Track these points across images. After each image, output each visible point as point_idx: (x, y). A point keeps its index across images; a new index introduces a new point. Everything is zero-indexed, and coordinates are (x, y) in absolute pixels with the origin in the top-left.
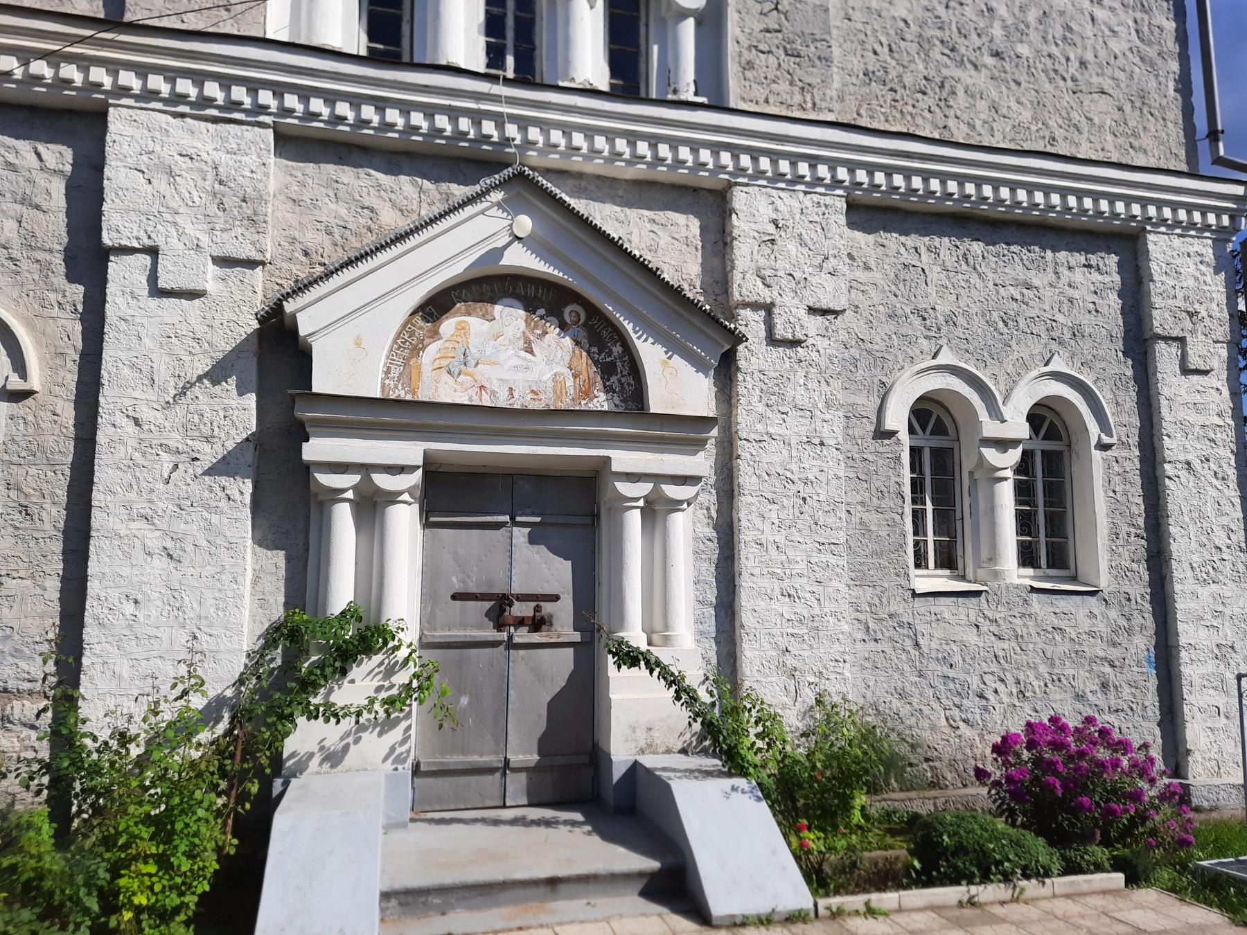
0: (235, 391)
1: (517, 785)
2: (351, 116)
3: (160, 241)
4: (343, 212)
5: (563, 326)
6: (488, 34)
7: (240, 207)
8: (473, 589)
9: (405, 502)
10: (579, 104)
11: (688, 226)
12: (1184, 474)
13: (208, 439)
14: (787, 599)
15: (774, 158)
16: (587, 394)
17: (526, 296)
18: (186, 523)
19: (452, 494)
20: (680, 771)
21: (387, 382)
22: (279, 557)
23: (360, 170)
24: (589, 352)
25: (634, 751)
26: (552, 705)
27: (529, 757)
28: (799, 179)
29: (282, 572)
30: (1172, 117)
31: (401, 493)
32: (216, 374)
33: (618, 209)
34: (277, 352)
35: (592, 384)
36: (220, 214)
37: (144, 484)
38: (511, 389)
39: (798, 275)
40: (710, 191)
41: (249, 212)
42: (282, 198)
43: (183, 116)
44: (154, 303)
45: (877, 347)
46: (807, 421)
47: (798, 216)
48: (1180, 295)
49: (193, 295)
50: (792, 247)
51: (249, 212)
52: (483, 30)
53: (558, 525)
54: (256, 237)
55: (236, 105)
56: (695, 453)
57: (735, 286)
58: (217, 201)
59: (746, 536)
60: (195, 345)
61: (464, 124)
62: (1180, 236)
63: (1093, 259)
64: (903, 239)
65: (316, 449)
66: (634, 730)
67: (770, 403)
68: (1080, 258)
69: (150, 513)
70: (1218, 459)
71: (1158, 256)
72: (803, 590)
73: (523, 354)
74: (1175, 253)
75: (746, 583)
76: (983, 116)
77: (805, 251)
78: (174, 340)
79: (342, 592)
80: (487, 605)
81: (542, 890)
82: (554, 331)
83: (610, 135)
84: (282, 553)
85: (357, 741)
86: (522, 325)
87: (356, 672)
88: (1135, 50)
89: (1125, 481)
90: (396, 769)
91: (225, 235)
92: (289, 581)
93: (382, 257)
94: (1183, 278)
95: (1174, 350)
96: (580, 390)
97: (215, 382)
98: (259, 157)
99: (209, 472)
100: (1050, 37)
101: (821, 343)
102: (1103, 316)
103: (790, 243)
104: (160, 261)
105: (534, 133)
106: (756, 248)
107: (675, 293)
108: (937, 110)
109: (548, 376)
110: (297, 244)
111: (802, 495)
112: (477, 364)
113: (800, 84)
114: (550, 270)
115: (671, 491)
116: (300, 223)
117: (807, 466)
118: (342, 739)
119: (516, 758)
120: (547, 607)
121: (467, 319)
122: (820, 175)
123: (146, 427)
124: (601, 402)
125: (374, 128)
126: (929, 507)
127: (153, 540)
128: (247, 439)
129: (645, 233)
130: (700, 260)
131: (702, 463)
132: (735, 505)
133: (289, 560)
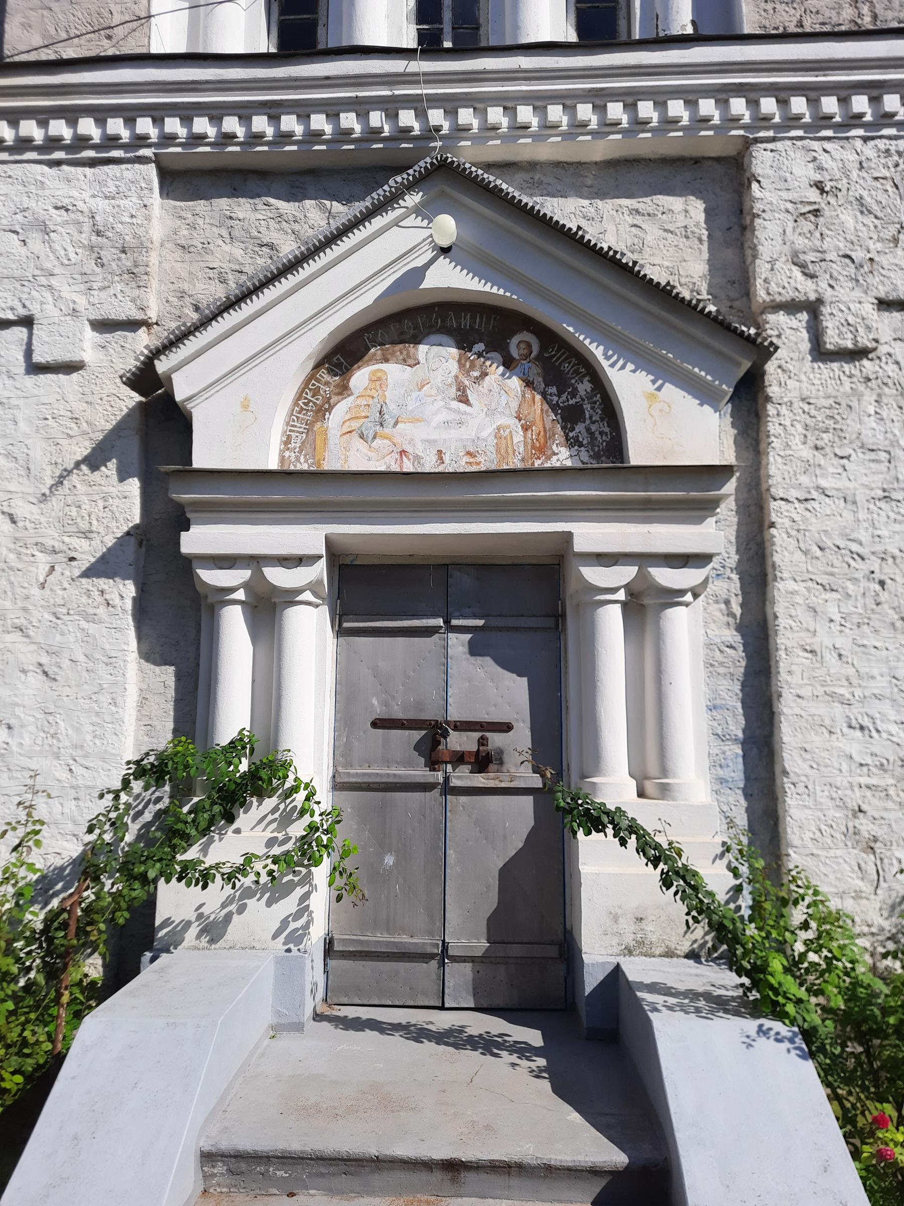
0: (115, 477)
1: (459, 978)
2: (240, 132)
3: (35, 309)
4: (238, 252)
5: (508, 363)
6: (419, 21)
7: (119, 259)
8: (399, 714)
10: (524, 66)
11: (688, 211)
13: (86, 534)
14: (858, 733)
15: (812, 95)
16: (542, 450)
17: (459, 328)
18: (62, 634)
19: (366, 591)
20: (676, 994)
21: (287, 454)
22: (168, 674)
23: (257, 201)
24: (544, 395)
25: (616, 950)
26: (505, 872)
27: (474, 943)
28: (855, 120)
29: (171, 693)
31: (299, 591)
32: (94, 461)
33: (586, 202)
34: (158, 427)
35: (548, 436)
36: (98, 270)
37: (19, 590)
38: (440, 452)
40: (718, 160)
41: (129, 264)
42: (169, 245)
43: (58, 163)
44: (31, 381)
46: (883, 467)
47: (854, 174)
49: (71, 367)
50: (848, 218)
51: (129, 264)
52: (413, 17)
53: (508, 629)
54: (136, 292)
55: (112, 141)
56: (700, 521)
57: (759, 282)
58: (95, 255)
59: (788, 639)
60: (73, 425)
61: (376, 118)
65: (197, 539)
66: (616, 919)
67: (820, 443)
69: (25, 622)
72: (885, 719)
73: (455, 404)
75: (789, 709)
77: (869, 220)
78: (51, 422)
79: (233, 716)
80: (417, 735)
81: (437, 1176)
82: (496, 371)
83: (568, 101)
84: (171, 669)
85: (241, 910)
86: (454, 367)
87: (244, 820)
90: (289, 950)
91: (103, 295)
92: (180, 702)
93: (270, 294)
96: (533, 447)
97: (94, 467)
99: (89, 573)
104: (35, 331)
105: (466, 116)
106: (791, 224)
107: (663, 294)
109: (488, 431)
110: (187, 299)
111: (877, 576)
112: (396, 423)
114: (487, 288)
115: (665, 576)
116: (190, 273)
117: (884, 532)
118: (224, 906)
119: (458, 943)
120: (496, 740)
121: (384, 366)
122: (888, 108)
123: (20, 524)
124: (562, 457)
125: (268, 143)
127: (28, 655)
128: (128, 533)
129: (625, 229)
130: (706, 255)
131: (716, 534)
132: (769, 596)
133: (179, 677)
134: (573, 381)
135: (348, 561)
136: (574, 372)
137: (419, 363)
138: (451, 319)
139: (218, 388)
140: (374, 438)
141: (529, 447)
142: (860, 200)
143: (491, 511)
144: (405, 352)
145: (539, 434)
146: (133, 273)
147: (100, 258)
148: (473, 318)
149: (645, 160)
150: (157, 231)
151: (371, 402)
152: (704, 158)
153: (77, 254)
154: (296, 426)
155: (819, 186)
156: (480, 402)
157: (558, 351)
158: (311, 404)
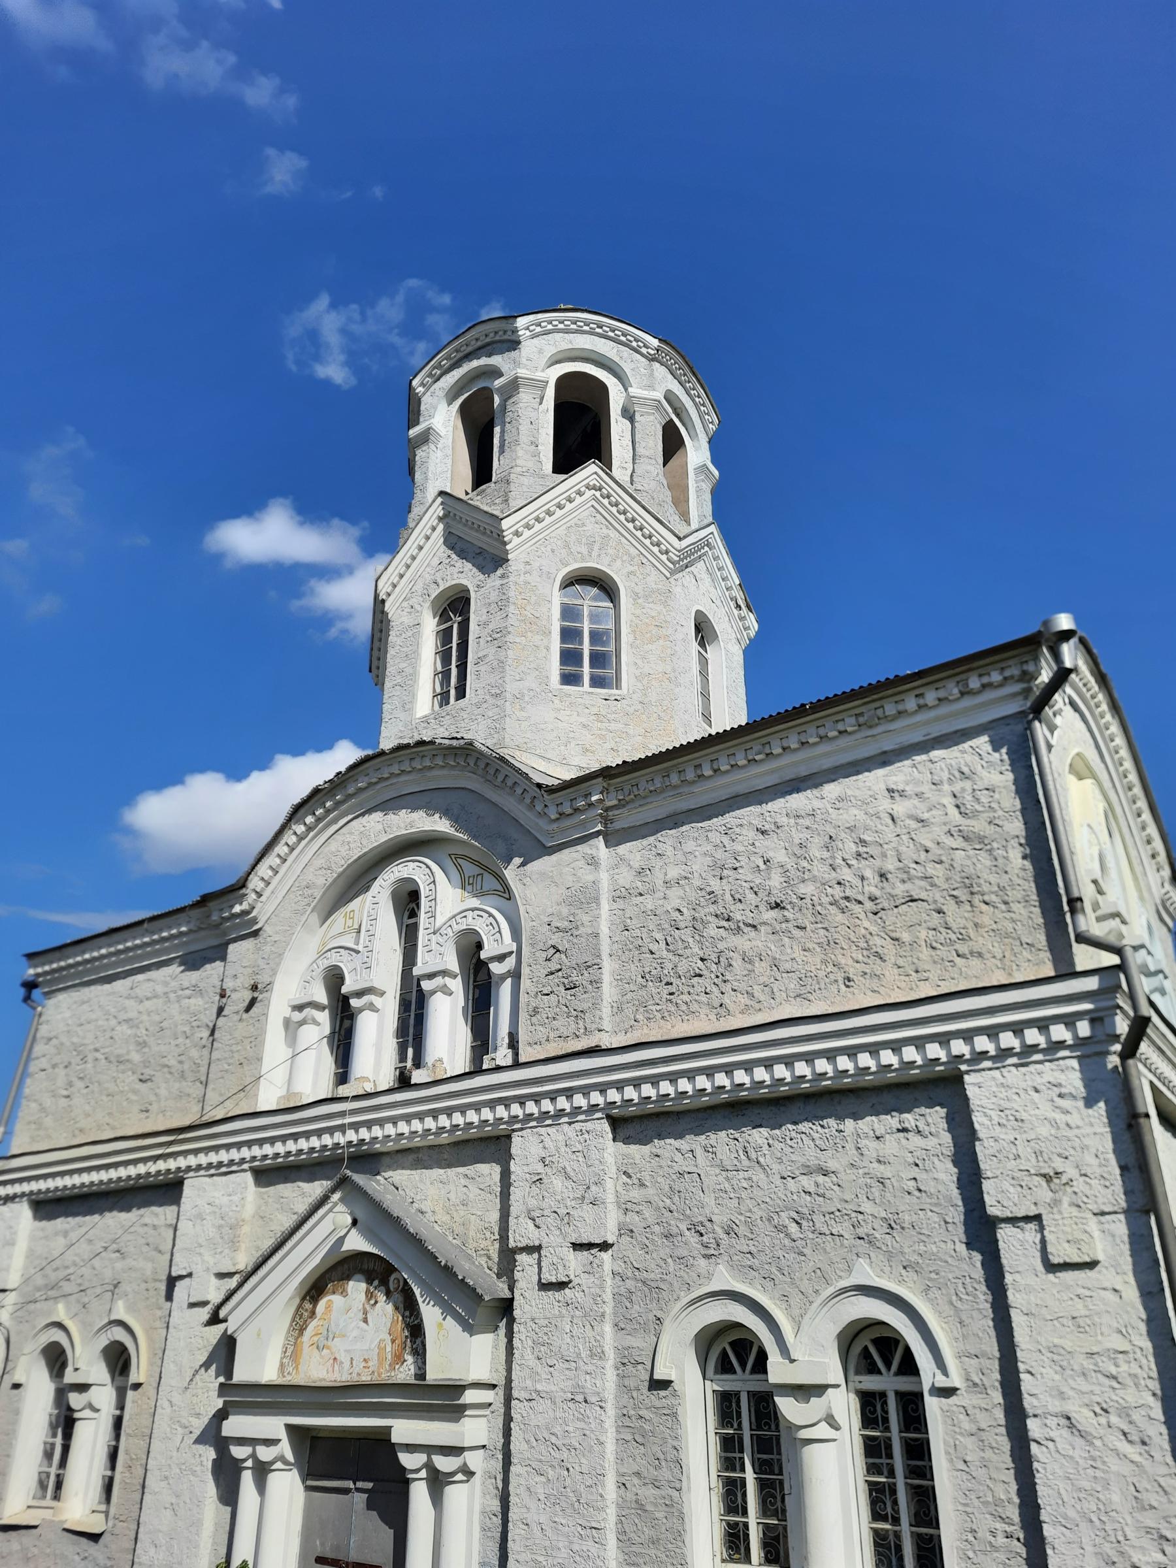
5: (388, 1294)
9: (461, 1482)
12: (1062, 1435)
30: (1019, 895)
31: (273, 1463)
33: (442, 1171)
39: (562, 1211)
43: (212, 1175)
45: (652, 1276)
48: (1024, 1150)
50: (558, 1183)
56: (457, 1420)
62: (1016, 1066)
63: (909, 1119)
64: (677, 1143)
68: (891, 1121)
70: (1124, 1412)
71: (984, 1102)
74: (1010, 1093)
76: (762, 979)
77: (569, 1184)
82: (382, 1298)
88: (954, 830)
89: (983, 1445)
94: (1026, 1125)
95: (1030, 1233)
100: (839, 861)
101: (585, 1280)
102: (930, 1196)
103: (575, 1174)
108: (715, 989)
113: (575, 1013)
117: (571, 1429)
126: (750, 1475)
142: (564, 1168)
150: (249, 1209)
155: (543, 1160)
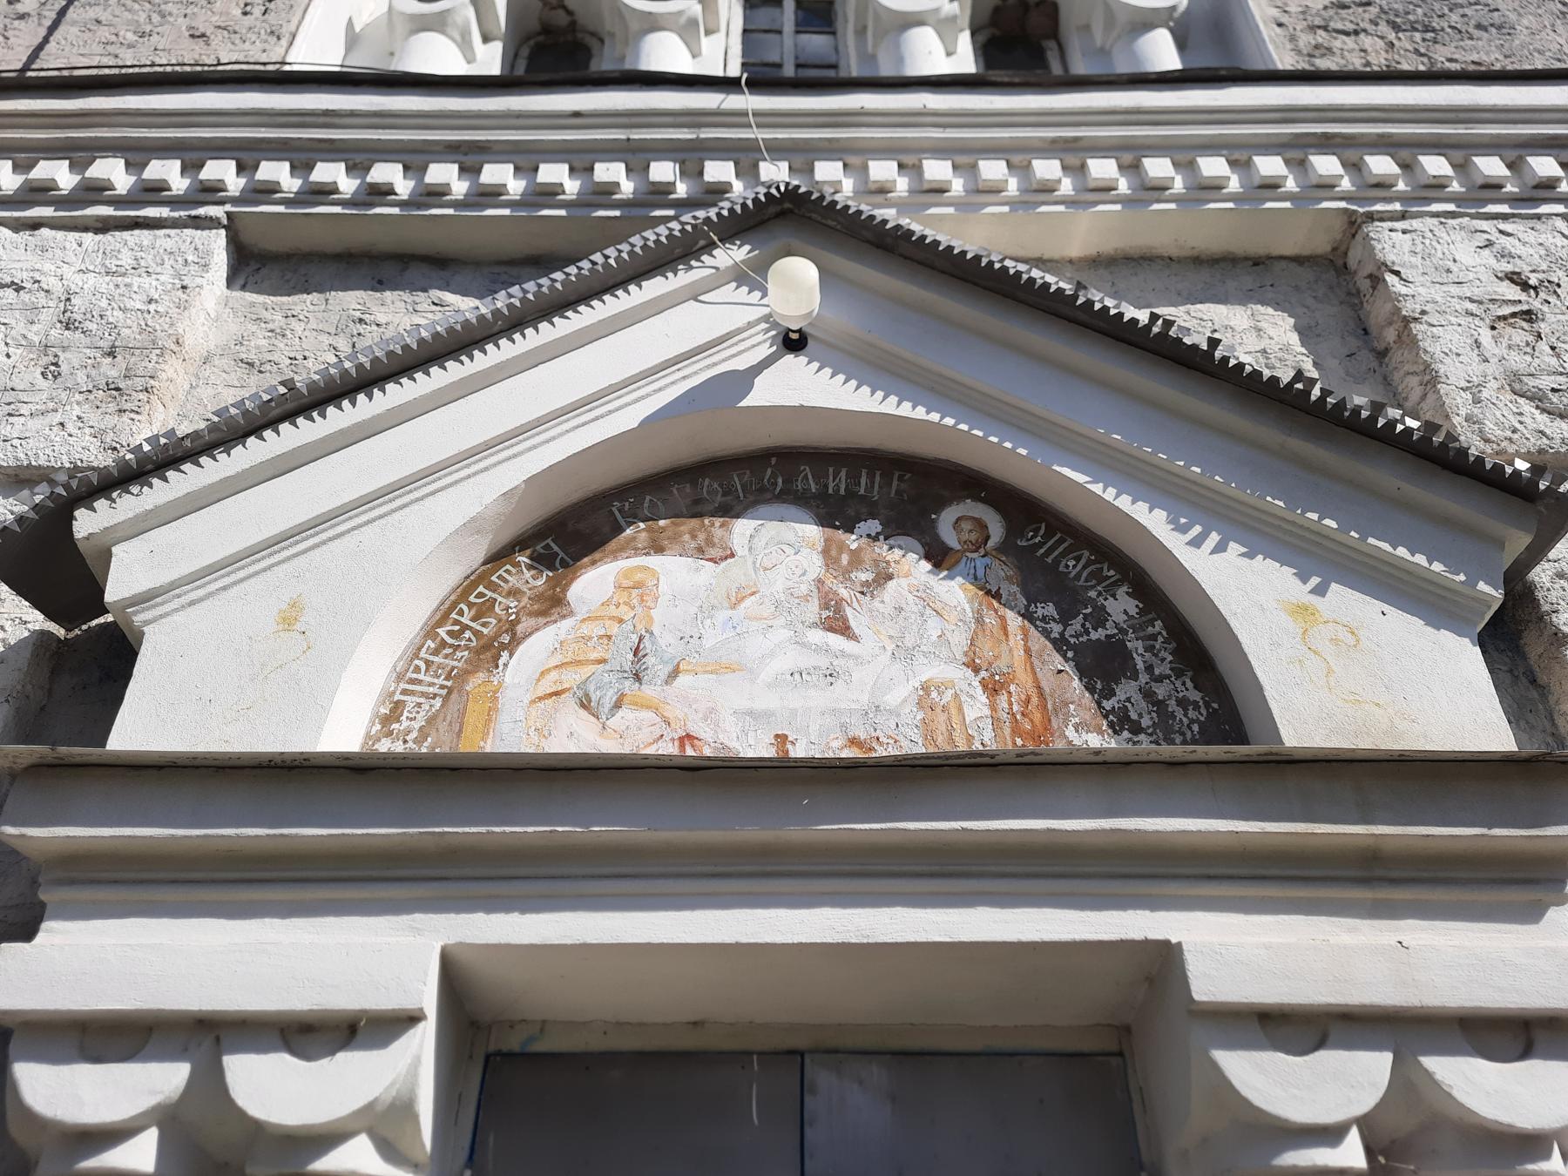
5: (939, 556)
23: (421, 297)
24: (1027, 616)
40: (1298, 260)
41: (113, 373)
42: (225, 362)
43: (35, 225)
55: (153, 192)
56: (1532, 913)
73: (818, 636)
82: (911, 567)
86: (814, 564)
98: (179, 276)
112: (675, 673)
121: (654, 561)
134: (1093, 594)
135: (513, 1043)
136: (1091, 575)
137: (732, 555)
138: (806, 477)
139: (227, 581)
140: (618, 705)
141: (1007, 731)
143: (932, 875)
144: (702, 536)
145: (1028, 700)
146: (117, 389)
147: (56, 364)
148: (854, 478)
149: (1161, 258)
151: (614, 629)
152: (1269, 258)
153: (8, 356)
154: (420, 682)
156: (878, 633)
157: (1047, 536)
158: (468, 634)
